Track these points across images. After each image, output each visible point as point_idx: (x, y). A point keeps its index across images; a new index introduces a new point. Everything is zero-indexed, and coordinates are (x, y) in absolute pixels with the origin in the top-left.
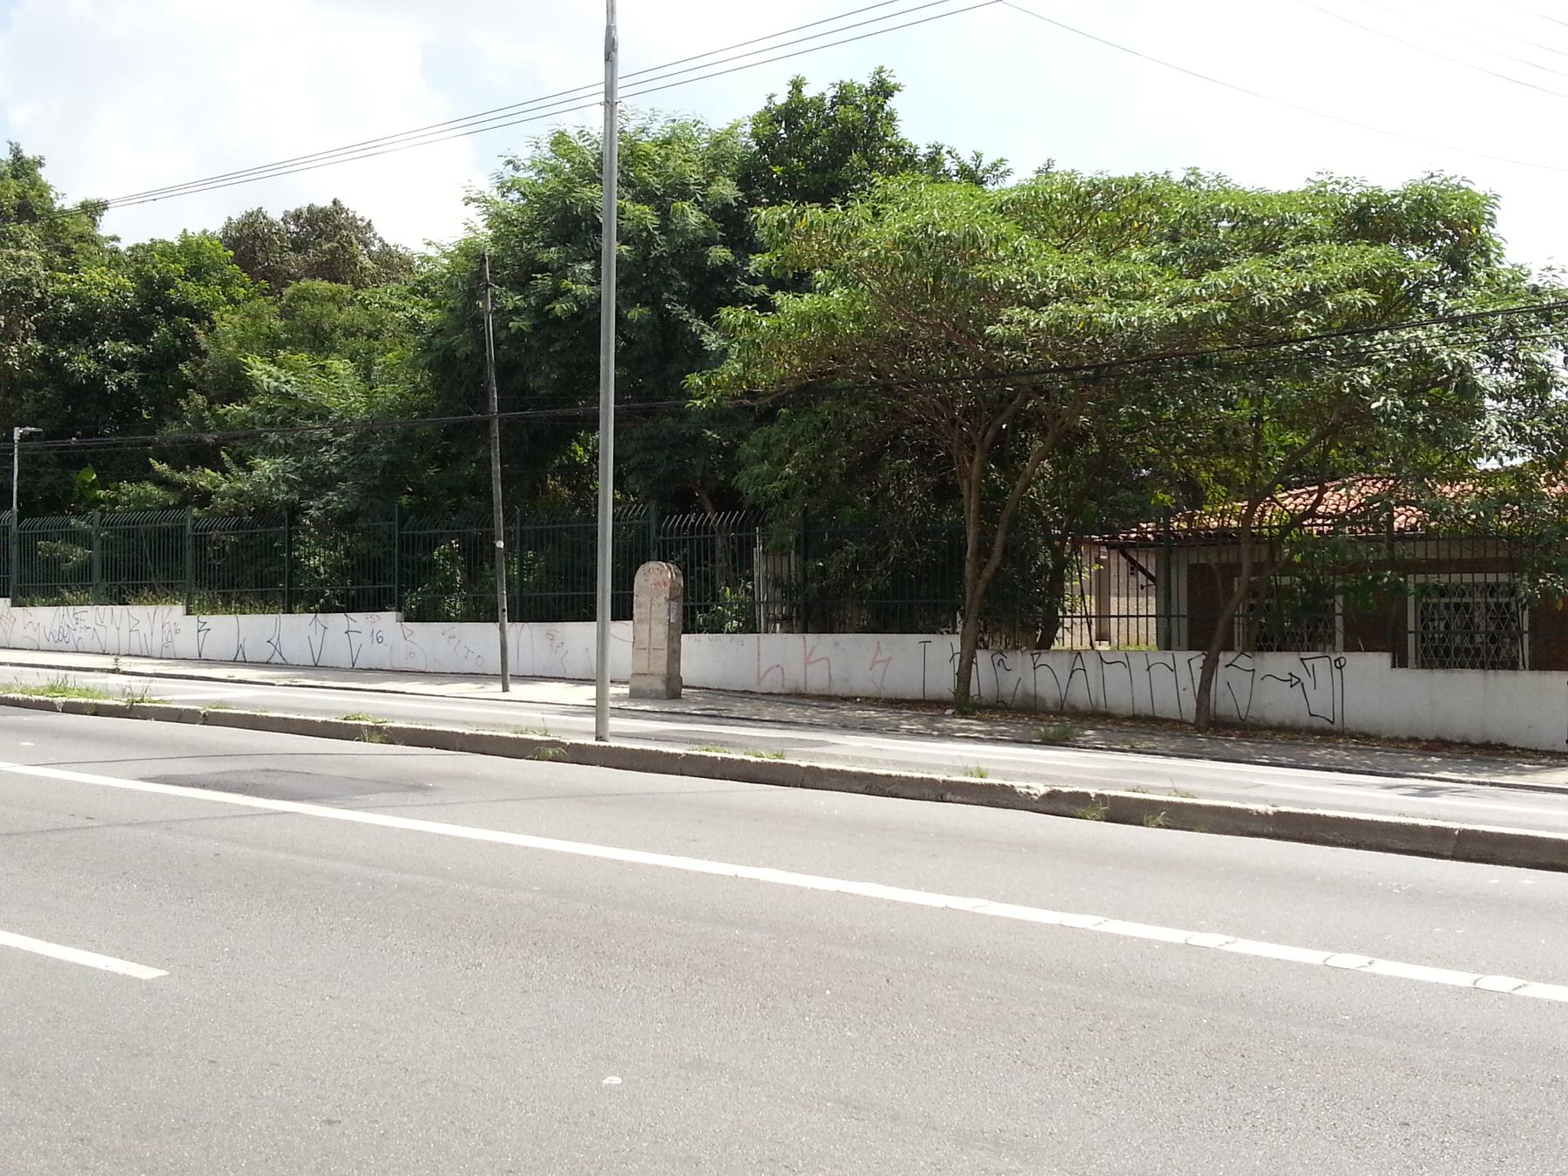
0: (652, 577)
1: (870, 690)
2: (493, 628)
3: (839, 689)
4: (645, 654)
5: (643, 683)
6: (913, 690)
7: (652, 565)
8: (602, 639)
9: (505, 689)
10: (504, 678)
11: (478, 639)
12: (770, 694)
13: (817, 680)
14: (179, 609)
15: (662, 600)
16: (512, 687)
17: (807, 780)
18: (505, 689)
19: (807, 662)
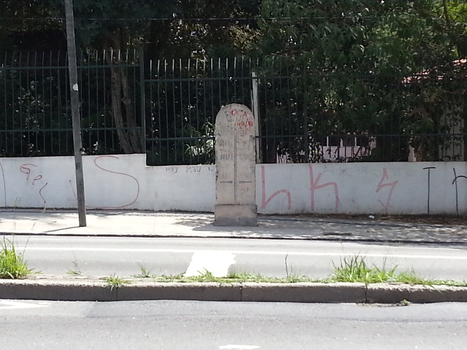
0: (236, 118)
1: (379, 208)
2: (68, 162)
3: (346, 208)
4: (230, 188)
5: (231, 212)
6: (419, 207)
7: (235, 107)
8: (79, 166)
9: (83, 224)
10: (81, 209)
11: (56, 170)
12: (277, 215)
13: (324, 201)
14: (142, 158)
15: (247, 138)
16: (90, 218)
17: (245, 295)
18: (83, 224)
19: (314, 186)
